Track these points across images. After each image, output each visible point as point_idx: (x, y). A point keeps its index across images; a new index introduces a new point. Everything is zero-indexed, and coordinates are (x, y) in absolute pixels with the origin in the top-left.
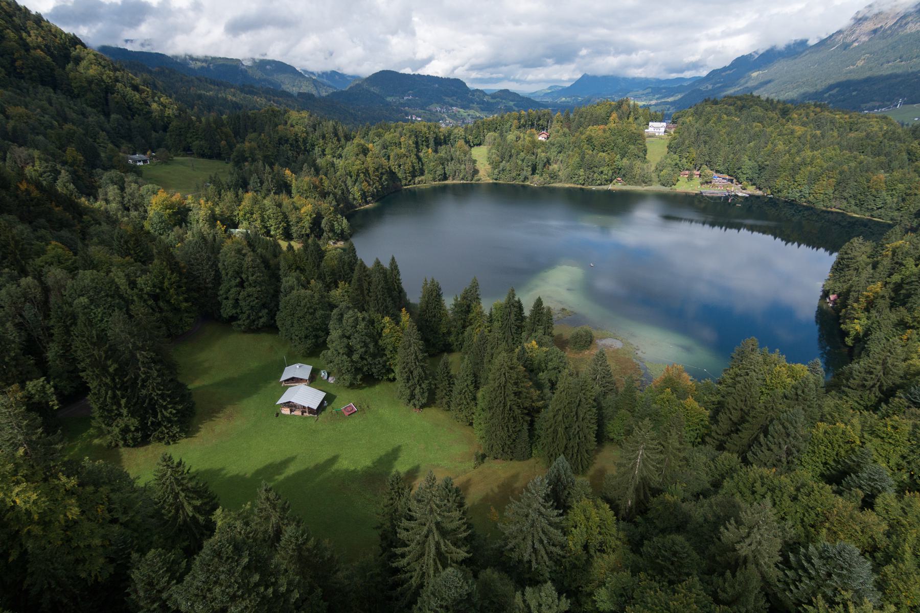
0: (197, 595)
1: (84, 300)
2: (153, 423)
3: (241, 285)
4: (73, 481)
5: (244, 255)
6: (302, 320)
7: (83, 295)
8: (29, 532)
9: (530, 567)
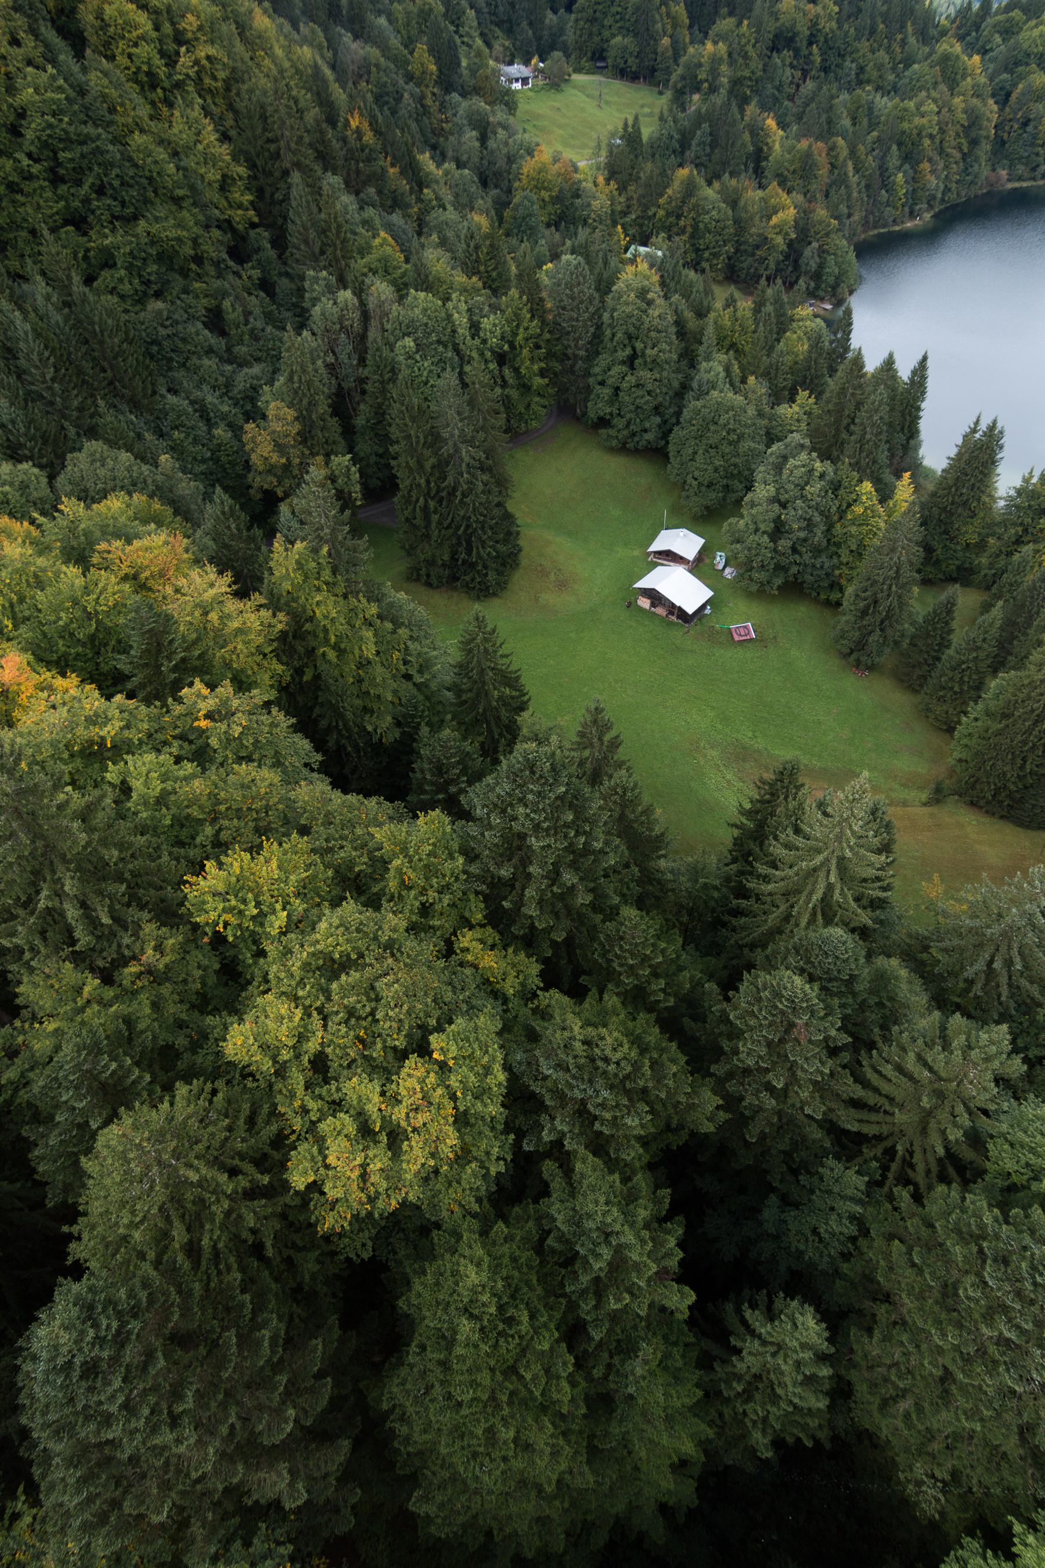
0: (496, 806)
1: (409, 342)
2: (464, 562)
3: (630, 362)
4: (373, 610)
5: (650, 303)
6: (713, 452)
7: (408, 335)
8: (324, 654)
9: (967, 991)
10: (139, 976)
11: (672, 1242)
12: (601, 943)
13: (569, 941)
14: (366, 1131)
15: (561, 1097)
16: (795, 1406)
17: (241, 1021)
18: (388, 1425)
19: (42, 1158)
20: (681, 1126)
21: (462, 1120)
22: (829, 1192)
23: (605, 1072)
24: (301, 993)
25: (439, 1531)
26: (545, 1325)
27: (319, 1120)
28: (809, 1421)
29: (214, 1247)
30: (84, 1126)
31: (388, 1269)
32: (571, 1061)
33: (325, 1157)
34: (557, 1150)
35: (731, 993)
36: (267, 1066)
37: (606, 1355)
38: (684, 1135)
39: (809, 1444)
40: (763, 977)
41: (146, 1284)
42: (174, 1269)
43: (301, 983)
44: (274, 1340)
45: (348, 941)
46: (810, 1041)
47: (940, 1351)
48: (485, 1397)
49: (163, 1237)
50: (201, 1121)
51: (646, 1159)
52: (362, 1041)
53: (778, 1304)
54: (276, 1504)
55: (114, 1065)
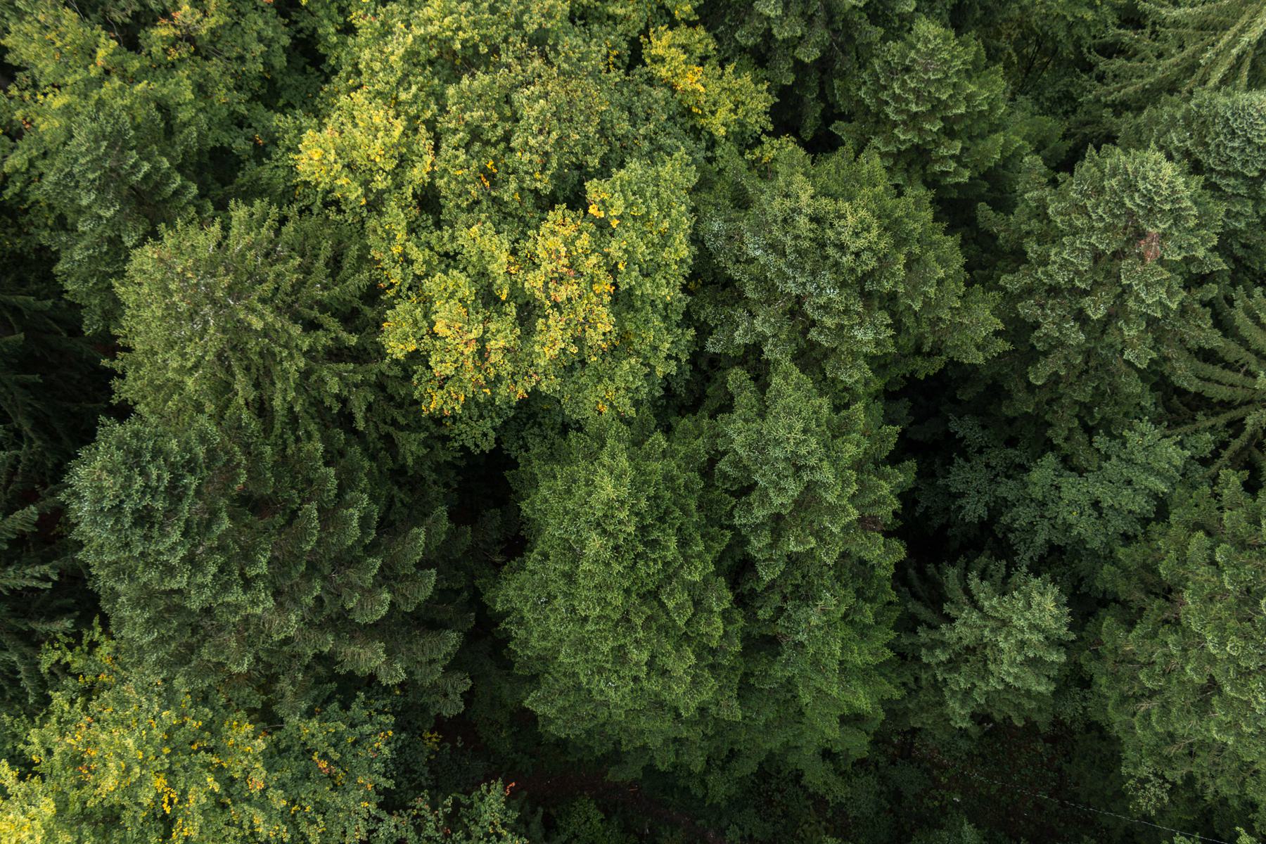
10: (174, 42)
11: (885, 488)
12: (875, 75)
13: (824, 65)
14: (488, 298)
15: (770, 292)
16: (1007, 685)
17: (320, 127)
18: (503, 625)
19: (69, 274)
20: (936, 351)
21: (622, 301)
22: (1130, 462)
23: (837, 264)
24: (403, 96)
25: (557, 730)
26: (699, 556)
27: (427, 275)
28: (1024, 701)
29: (291, 409)
30: (115, 242)
31: (516, 466)
32: (789, 241)
33: (432, 324)
34: (754, 361)
35: (1061, 176)
36: (356, 193)
37: (777, 598)
38: (938, 363)
39: (1019, 723)
40: (1116, 157)
41: (203, 439)
42: (240, 427)
43: (404, 81)
44: (364, 522)
45: (475, 24)
46: (1161, 261)
47: (1212, 660)
48: (616, 616)
49: (224, 390)
50: (267, 255)
51: (877, 384)
52: (491, 176)
53: (1017, 578)
54: (372, 678)
55: (146, 167)
